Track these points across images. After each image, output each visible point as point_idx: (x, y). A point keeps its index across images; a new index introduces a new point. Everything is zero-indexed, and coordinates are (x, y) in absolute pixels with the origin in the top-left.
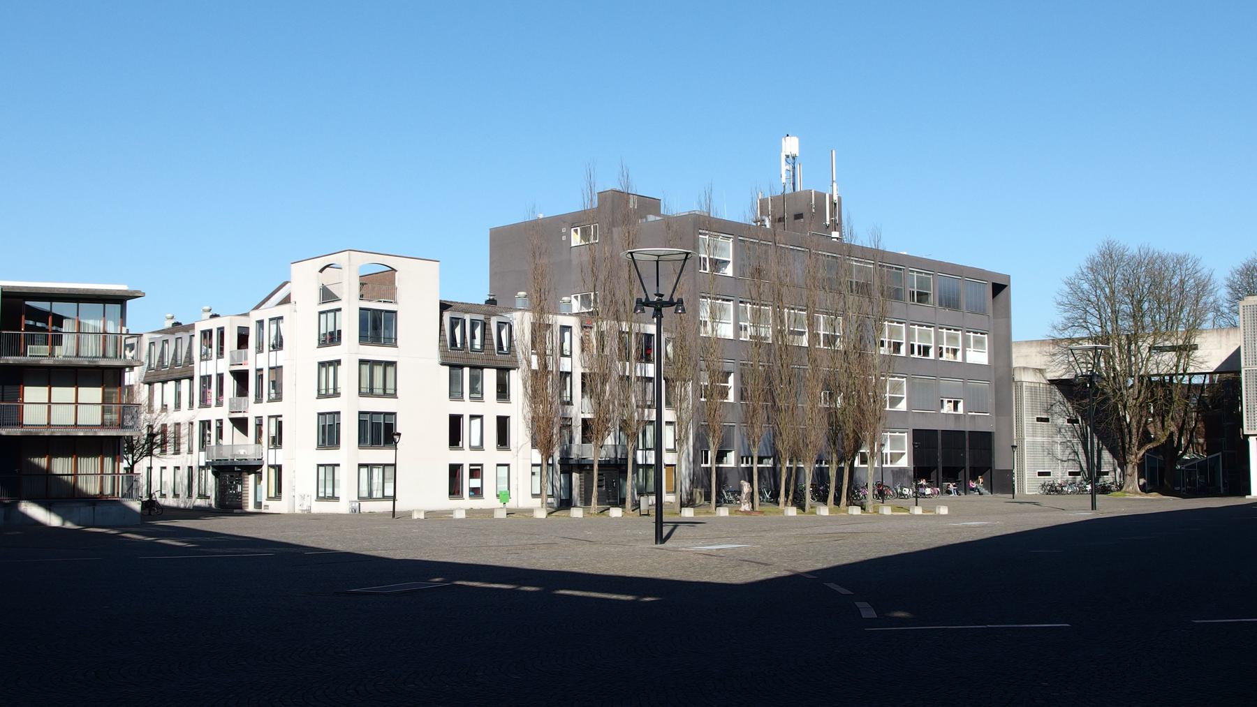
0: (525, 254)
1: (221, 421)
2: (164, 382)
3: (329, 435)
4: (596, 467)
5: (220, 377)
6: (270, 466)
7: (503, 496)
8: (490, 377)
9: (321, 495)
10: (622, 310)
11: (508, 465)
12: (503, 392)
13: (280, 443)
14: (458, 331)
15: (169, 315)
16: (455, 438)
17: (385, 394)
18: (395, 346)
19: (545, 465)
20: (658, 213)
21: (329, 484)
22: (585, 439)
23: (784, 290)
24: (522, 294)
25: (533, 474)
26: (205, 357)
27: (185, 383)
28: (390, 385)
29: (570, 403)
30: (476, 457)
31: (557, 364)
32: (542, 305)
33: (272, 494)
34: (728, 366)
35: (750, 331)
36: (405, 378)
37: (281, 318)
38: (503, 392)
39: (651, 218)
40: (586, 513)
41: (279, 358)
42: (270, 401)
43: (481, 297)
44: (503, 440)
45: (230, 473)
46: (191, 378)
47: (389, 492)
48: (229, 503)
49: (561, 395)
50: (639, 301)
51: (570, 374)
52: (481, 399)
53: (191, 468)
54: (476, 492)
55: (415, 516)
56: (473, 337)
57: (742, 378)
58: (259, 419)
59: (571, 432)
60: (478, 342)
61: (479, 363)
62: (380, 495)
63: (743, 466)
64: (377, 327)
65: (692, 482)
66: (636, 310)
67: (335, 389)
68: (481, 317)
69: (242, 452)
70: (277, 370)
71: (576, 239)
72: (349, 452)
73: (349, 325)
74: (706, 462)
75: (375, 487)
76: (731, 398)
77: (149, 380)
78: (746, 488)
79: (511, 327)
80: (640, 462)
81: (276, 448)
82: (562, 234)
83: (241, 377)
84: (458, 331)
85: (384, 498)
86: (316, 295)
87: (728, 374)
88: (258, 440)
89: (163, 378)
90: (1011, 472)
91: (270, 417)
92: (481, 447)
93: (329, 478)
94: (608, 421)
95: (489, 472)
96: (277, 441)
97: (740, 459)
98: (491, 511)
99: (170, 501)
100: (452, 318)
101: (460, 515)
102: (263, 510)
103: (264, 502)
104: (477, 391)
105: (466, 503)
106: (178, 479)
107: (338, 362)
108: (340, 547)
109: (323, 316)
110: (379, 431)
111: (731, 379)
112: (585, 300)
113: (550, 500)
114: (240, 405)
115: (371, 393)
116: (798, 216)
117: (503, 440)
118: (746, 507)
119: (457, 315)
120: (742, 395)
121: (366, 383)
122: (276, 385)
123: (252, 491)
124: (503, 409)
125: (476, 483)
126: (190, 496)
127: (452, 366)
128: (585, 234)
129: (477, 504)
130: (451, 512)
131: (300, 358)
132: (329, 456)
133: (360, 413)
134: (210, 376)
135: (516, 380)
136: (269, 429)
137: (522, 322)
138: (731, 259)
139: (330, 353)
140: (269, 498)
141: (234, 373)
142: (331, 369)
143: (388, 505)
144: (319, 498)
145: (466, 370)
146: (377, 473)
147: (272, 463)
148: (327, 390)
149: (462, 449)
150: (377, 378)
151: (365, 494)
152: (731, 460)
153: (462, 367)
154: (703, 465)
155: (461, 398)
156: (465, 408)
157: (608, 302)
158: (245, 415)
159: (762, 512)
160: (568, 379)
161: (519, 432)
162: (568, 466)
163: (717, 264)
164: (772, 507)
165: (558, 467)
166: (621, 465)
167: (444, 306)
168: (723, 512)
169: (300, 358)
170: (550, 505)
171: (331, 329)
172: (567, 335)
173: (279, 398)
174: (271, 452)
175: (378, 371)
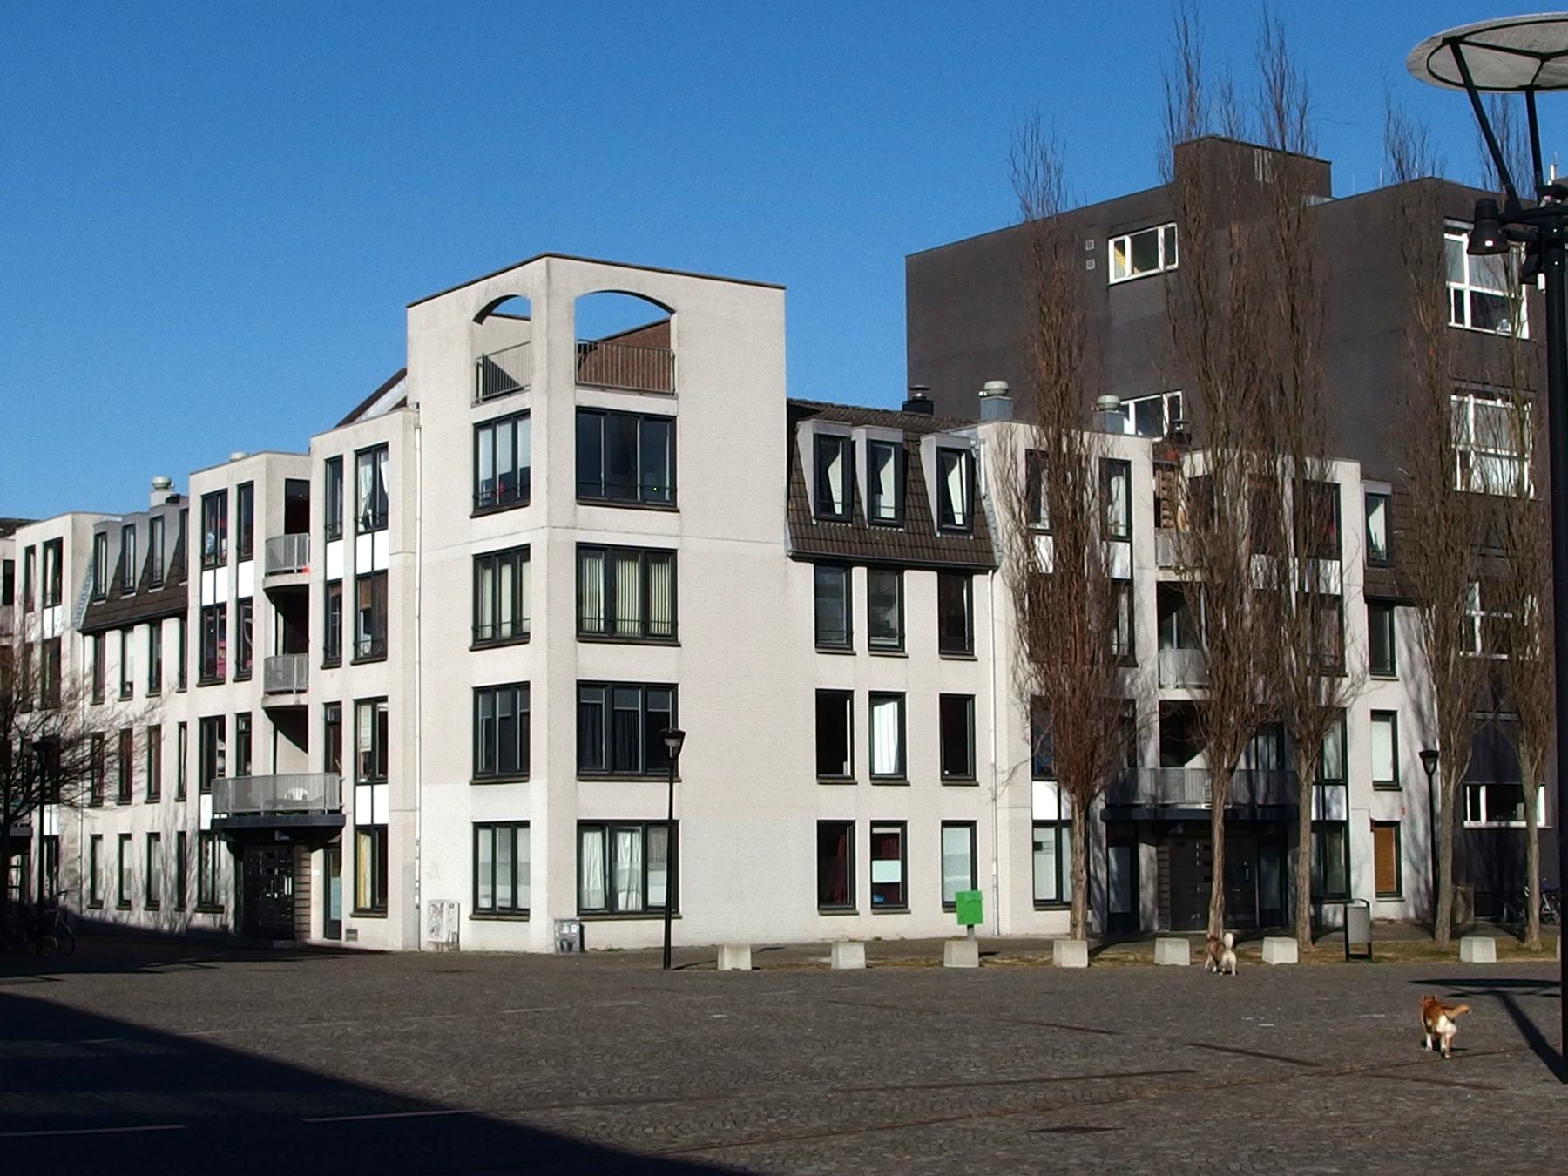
0: (997, 312)
1: (245, 717)
2: (126, 628)
3: (501, 745)
4: (1218, 825)
5: (245, 604)
6: (360, 830)
7: (961, 905)
8: (921, 592)
9: (485, 903)
11: (971, 824)
12: (956, 636)
13: (384, 769)
14: (835, 473)
15: (160, 480)
16: (832, 758)
17: (647, 637)
18: (672, 507)
20: (1324, 187)
21: (504, 874)
22: (1175, 751)
24: (996, 385)
25: (1037, 846)
26: (213, 559)
27: (170, 627)
28: (660, 611)
29: (1130, 661)
32: (1059, 406)
33: (365, 902)
36: (697, 598)
37: (383, 447)
38: (956, 636)
39: (1313, 200)
41: (379, 551)
42: (358, 661)
43: (892, 394)
44: (958, 760)
45: (271, 843)
46: (182, 616)
47: (658, 896)
48: (267, 927)
52: (898, 650)
53: (182, 835)
54: (890, 897)
55: (727, 963)
56: (875, 488)
58: (334, 708)
60: (887, 499)
61: (890, 555)
62: (635, 903)
64: (626, 459)
67: (517, 620)
68: (896, 435)
69: (298, 794)
70: (373, 583)
71: (1121, 267)
72: (551, 793)
73: (550, 453)
74: (1475, 816)
75: (623, 882)
77: (95, 624)
79: (972, 465)
81: (372, 782)
83: (291, 602)
84: (835, 473)
85: (647, 911)
86: (465, 381)
88: (332, 762)
89: (123, 616)
91: (359, 703)
92: (899, 777)
93: (504, 857)
95: (922, 843)
96: (375, 767)
98: (934, 948)
99: (139, 917)
100: (818, 438)
101: (851, 959)
102: (344, 942)
103: (348, 922)
104: (888, 636)
105: (865, 922)
106: (157, 865)
107: (523, 552)
108: (450, 1088)
109: (486, 436)
110: (631, 733)
114: (289, 676)
115: (609, 633)
117: (958, 760)
119: (835, 429)
121: (595, 609)
122: (374, 620)
123: (322, 894)
124: (956, 677)
125: (888, 871)
126: (181, 906)
128: (1144, 256)
129: (891, 926)
130: (825, 948)
131: (428, 545)
132: (502, 802)
133: (582, 685)
134: (222, 607)
135: (993, 602)
136: (356, 735)
137: (1000, 447)
139: (501, 530)
140: (358, 912)
141: (274, 594)
142: (507, 572)
143: (648, 933)
144: (478, 913)
145: (859, 575)
146: (628, 844)
147: (364, 819)
148: (497, 624)
149: (851, 780)
150: (629, 593)
151: (595, 900)
153: (846, 565)
154: (1468, 824)
155: (846, 648)
156: (857, 672)
158: (303, 700)
160: (1124, 599)
161: (1001, 735)
162: (1128, 824)
167: (797, 412)
169: (428, 545)
171: (504, 467)
172: (1118, 485)
173: (379, 653)
174: (364, 791)
175: (629, 576)
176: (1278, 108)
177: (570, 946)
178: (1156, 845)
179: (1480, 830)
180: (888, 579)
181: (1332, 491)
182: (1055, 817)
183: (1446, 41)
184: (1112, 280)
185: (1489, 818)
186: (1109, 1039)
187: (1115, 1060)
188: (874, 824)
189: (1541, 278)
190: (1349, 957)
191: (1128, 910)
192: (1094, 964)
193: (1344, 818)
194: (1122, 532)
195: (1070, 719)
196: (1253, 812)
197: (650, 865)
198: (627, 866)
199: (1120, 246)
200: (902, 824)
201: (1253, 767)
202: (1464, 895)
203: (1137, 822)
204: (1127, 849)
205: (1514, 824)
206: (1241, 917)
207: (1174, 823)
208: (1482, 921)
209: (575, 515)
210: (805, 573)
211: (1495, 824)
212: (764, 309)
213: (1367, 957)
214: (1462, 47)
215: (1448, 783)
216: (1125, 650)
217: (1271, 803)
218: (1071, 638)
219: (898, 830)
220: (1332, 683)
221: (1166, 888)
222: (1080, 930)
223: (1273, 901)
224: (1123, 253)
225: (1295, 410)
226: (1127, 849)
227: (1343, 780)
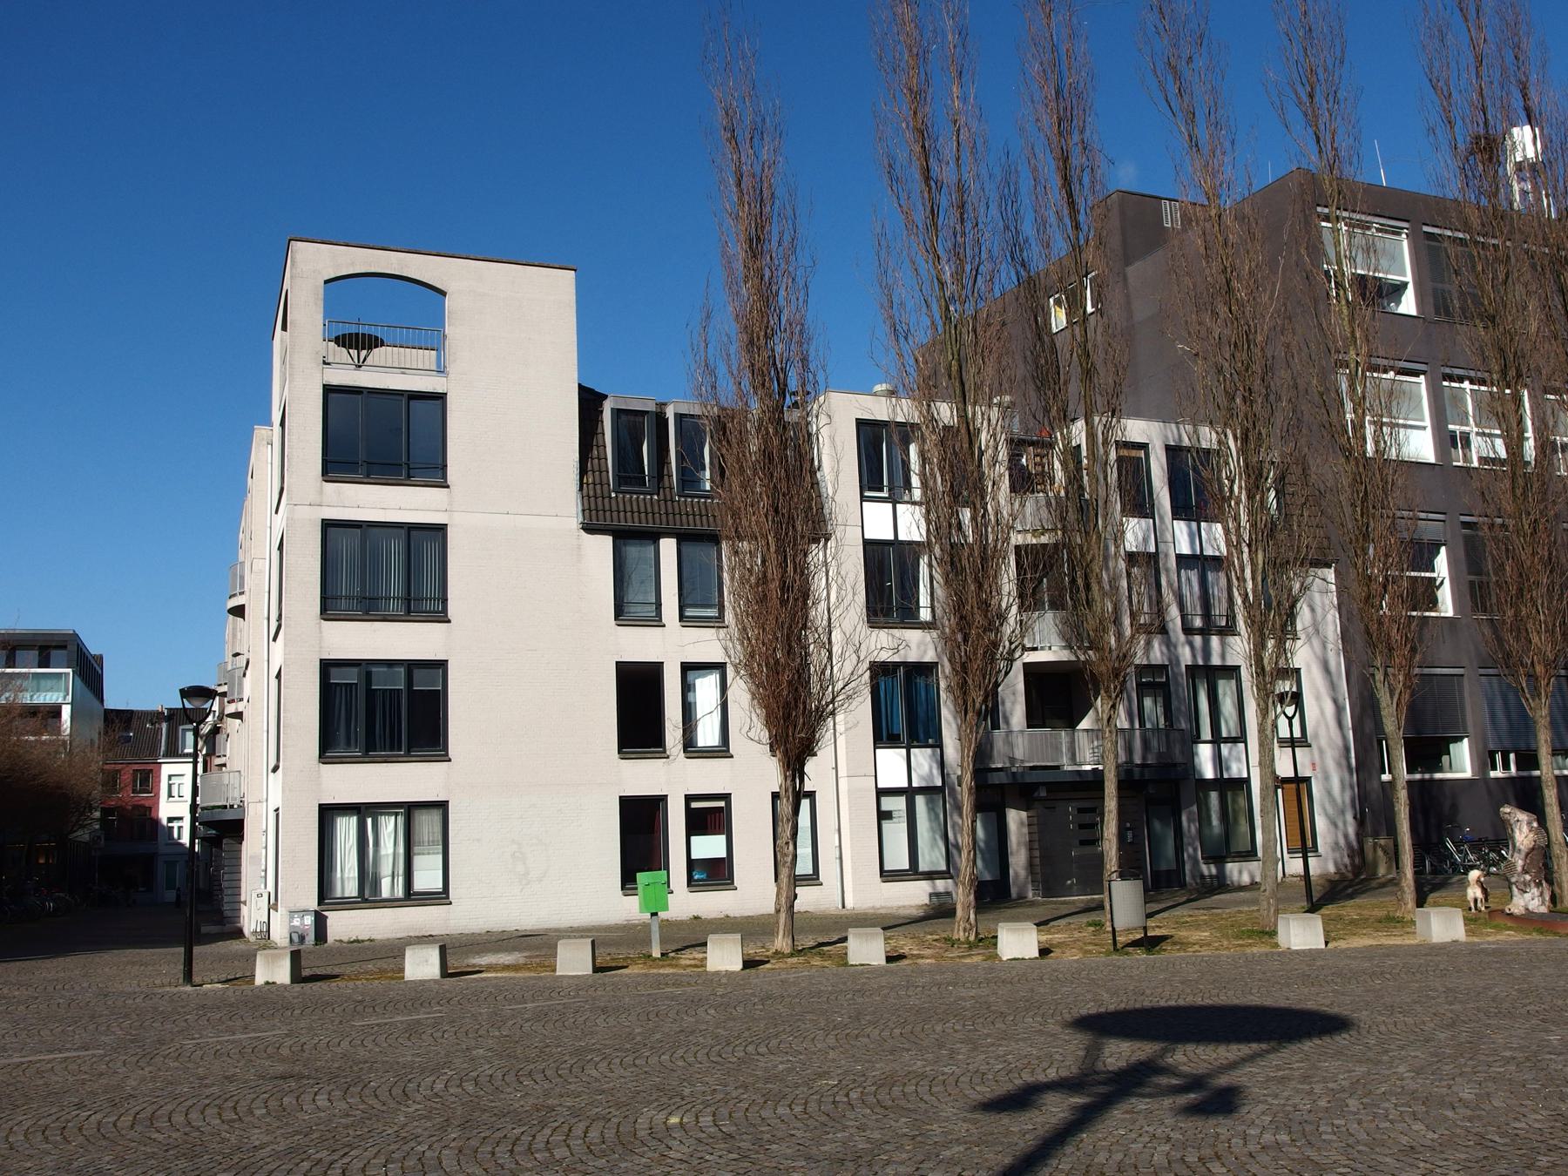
4: (1110, 788)
25: (883, 816)
30: (706, 777)
34: (1430, 528)
54: (716, 873)
61: (702, 526)
76: (1447, 605)
80: (1209, 773)
92: (722, 751)
97: (1485, 759)
111: (1442, 562)
120: (1474, 592)
125: (709, 847)
127: (622, 537)
128: (1074, 304)
145: (668, 547)
152: (1462, 762)
153: (654, 537)
168: (1443, 926)
176: (921, 133)
177: (302, 938)
179: (1511, 779)
180: (633, 551)
182: (905, 785)
185: (1518, 769)
188: (689, 799)
197: (416, 849)
198: (391, 851)
200: (726, 797)
205: (1438, 776)
209: (321, 492)
210: (603, 545)
211: (1418, 776)
212: (548, 296)
219: (722, 804)
220: (1223, 644)
221: (1037, 853)
223: (1167, 863)
226: (993, 815)
227: (1241, 738)
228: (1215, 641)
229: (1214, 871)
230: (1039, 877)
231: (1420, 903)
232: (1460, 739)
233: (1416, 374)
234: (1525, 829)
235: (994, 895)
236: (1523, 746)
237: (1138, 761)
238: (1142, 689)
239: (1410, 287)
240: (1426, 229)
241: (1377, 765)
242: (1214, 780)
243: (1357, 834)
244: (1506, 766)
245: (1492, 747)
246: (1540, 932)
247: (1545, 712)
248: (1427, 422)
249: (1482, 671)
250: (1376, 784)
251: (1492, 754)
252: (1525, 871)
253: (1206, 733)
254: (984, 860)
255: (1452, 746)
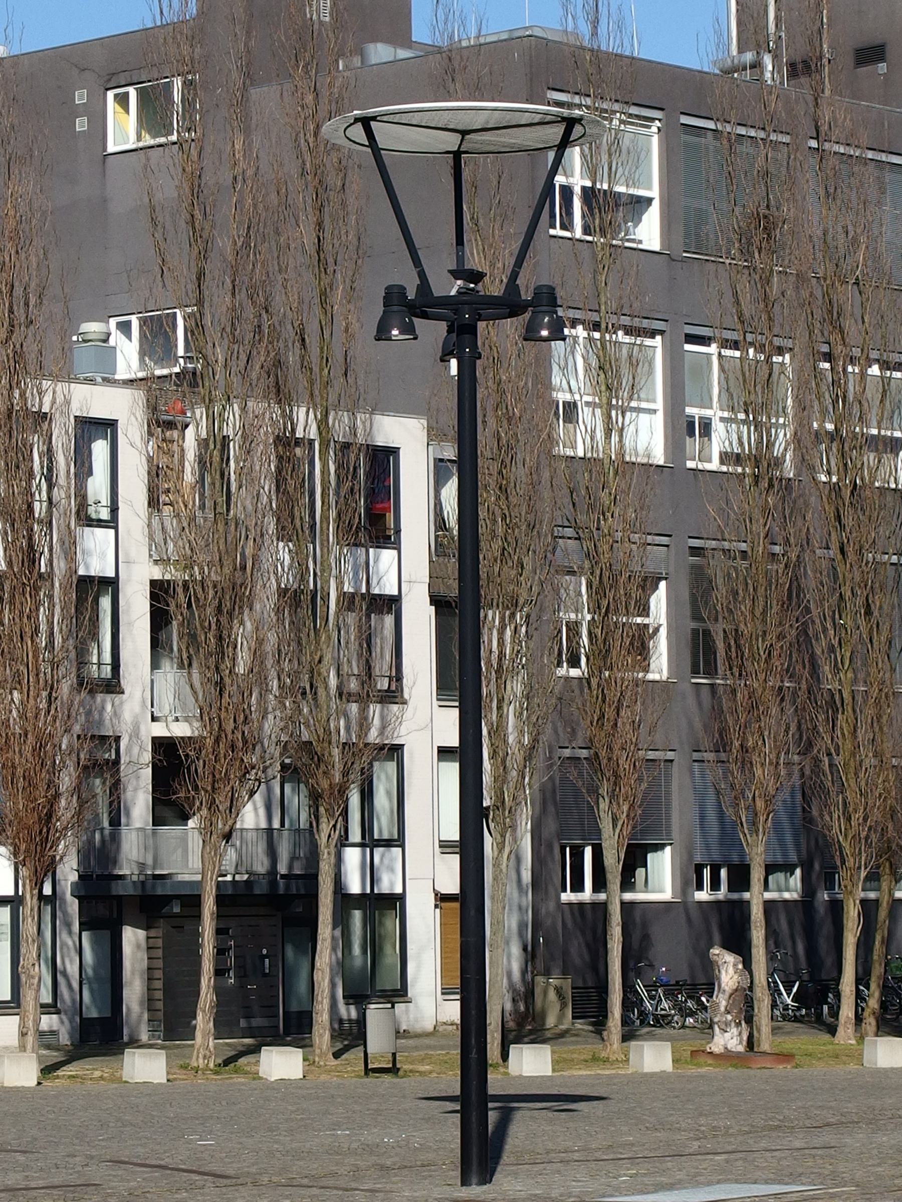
4: (209, 906)
10: (292, 358)
19: (31, 902)
22: (169, 807)
23: (847, 295)
29: (113, 686)
31: (70, 547)
34: (656, 557)
35: (722, 438)
39: (380, 53)
40: (180, 1066)
49: (82, 661)
50: (394, 297)
51: (110, 584)
57: (698, 600)
59: (116, 787)
63: (703, 896)
65: (530, 954)
66: (382, 334)
71: (123, 129)
74: (578, 886)
76: (660, 665)
78: (729, 972)
80: (354, 886)
82: (75, 112)
87: (649, 583)
90: (200, 896)
94: (250, 744)
97: (691, 874)
111: (659, 601)
112: (156, 339)
113: (48, 1022)
116: (870, 54)
118: (729, 1039)
120: (699, 652)
128: (154, 112)
138: (654, 192)
152: (661, 879)
154: (568, 896)
157: (246, 330)
159: (785, 1057)
160: (105, 603)
162: (107, 903)
163: (609, 209)
164: (804, 1040)
165: (73, 906)
166: (289, 898)
168: (654, 1057)
170: (46, 1039)
172: (100, 449)
178: (147, 928)
179: (581, 905)
181: (383, 459)
183: (357, 120)
184: (111, 148)
185: (730, 889)
186: (21, 1158)
187: (19, 1176)
189: (454, 363)
190: (367, 1071)
191: (108, 1014)
192: (45, 1083)
193: (398, 890)
194: (105, 514)
195: (20, 771)
196: (273, 883)
199: (123, 100)
201: (276, 824)
202: (559, 991)
203: (120, 898)
204: (107, 934)
206: (257, 1022)
207: (167, 899)
208: (580, 1025)
213: (393, 1070)
214: (372, 123)
215: (501, 850)
216: (107, 671)
217: (297, 872)
218: (22, 668)
221: (159, 984)
222: (30, 1039)
224: (127, 110)
225: (322, 370)
226: (107, 934)
227: (398, 841)
228: (375, 710)
229: (354, 1014)
230: (160, 1015)
231: (626, 1038)
232: (661, 847)
233: (652, 334)
234: (731, 970)
235: (100, 1035)
236: (735, 859)
237: (282, 869)
238: (290, 773)
239: (656, 204)
240: (685, 120)
241: (558, 881)
242: (363, 895)
243: (524, 972)
244: (715, 885)
245: (698, 859)
246: (735, 1066)
247: (761, 849)
248: (659, 405)
249: (696, 756)
250: (552, 905)
251: (699, 869)
252: (728, 1012)
253: (355, 835)
254: (92, 991)
255: (649, 856)
